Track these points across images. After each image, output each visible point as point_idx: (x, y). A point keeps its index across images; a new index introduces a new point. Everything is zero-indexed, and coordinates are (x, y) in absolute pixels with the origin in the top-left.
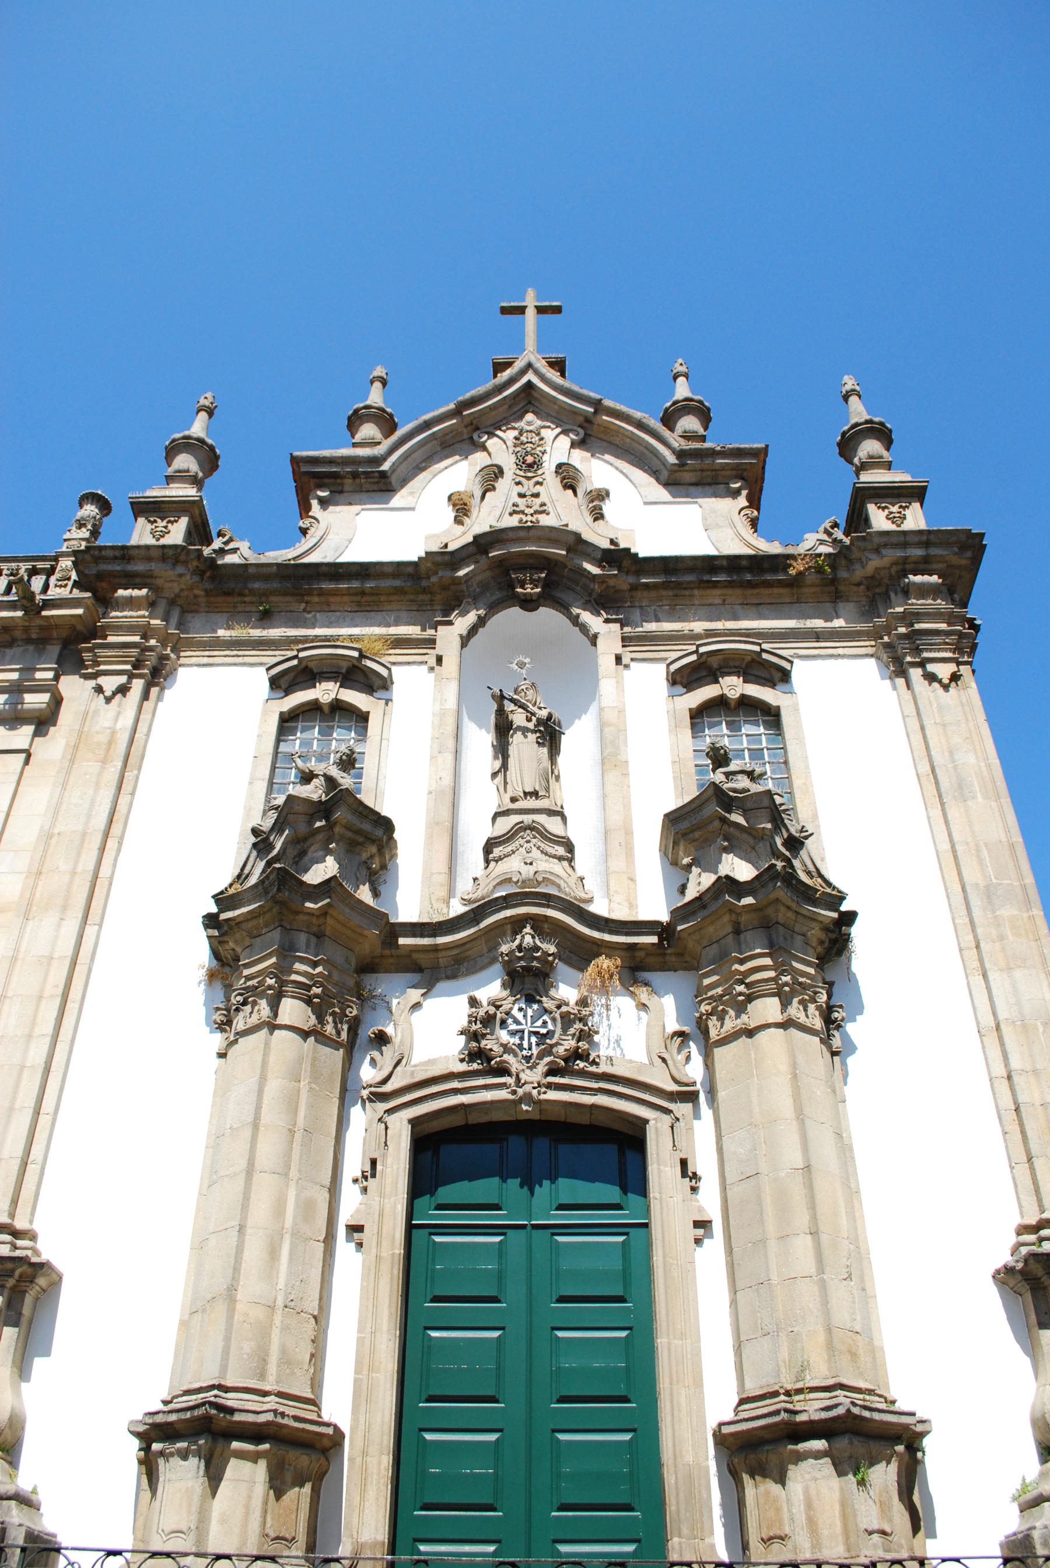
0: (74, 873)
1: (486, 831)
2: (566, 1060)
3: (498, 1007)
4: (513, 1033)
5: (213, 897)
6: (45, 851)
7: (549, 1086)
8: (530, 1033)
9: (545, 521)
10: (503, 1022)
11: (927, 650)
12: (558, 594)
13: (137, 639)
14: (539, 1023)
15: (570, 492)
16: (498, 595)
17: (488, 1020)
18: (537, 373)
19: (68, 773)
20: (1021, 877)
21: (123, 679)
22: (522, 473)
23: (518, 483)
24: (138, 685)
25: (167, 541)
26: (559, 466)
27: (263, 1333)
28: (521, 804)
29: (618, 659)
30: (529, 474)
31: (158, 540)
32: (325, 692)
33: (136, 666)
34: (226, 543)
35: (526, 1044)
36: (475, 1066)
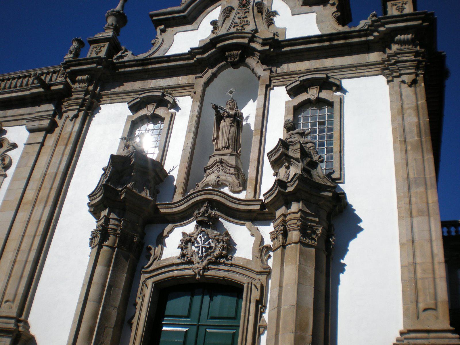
4: (196, 247)
5: (88, 196)
8: (202, 247)
11: (402, 70)
22: (240, 9)
24: (81, 114)
30: (243, 9)
31: (97, 55)
32: (313, 94)
34: (123, 53)
35: (200, 252)
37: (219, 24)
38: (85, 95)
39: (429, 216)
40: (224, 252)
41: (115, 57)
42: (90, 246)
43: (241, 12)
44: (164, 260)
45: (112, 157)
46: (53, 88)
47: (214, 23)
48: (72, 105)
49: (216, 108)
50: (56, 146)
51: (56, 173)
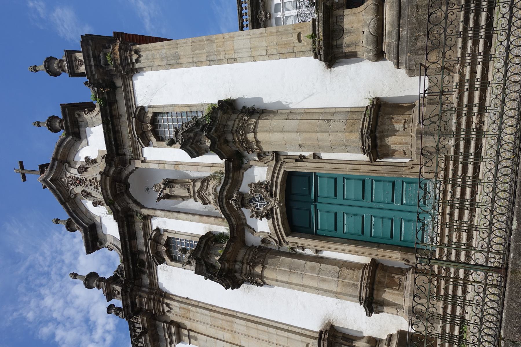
0: (222, 320)
1: (200, 203)
2: (268, 192)
3: (253, 211)
6: (216, 327)
7: (276, 197)
9: (99, 179)
10: (258, 209)
12: (123, 178)
13: (152, 301)
14: (257, 199)
15: (88, 169)
16: (126, 196)
17: (257, 213)
18: (48, 177)
19: (194, 320)
20: (203, 41)
21: (165, 305)
23: (87, 186)
24: (166, 301)
25: (120, 291)
26: (79, 172)
27: (345, 285)
28: (192, 194)
29: (142, 162)
33: (160, 302)
36: (271, 217)
37: (95, 200)
38: (151, 299)
39: (233, 134)
40: (263, 186)
41: (121, 278)
42: (262, 285)
43: (86, 184)
44: (270, 230)
45: (196, 273)
46: (146, 326)
47: (95, 204)
48: (159, 308)
49: (159, 199)
50: (190, 319)
51: (211, 316)
